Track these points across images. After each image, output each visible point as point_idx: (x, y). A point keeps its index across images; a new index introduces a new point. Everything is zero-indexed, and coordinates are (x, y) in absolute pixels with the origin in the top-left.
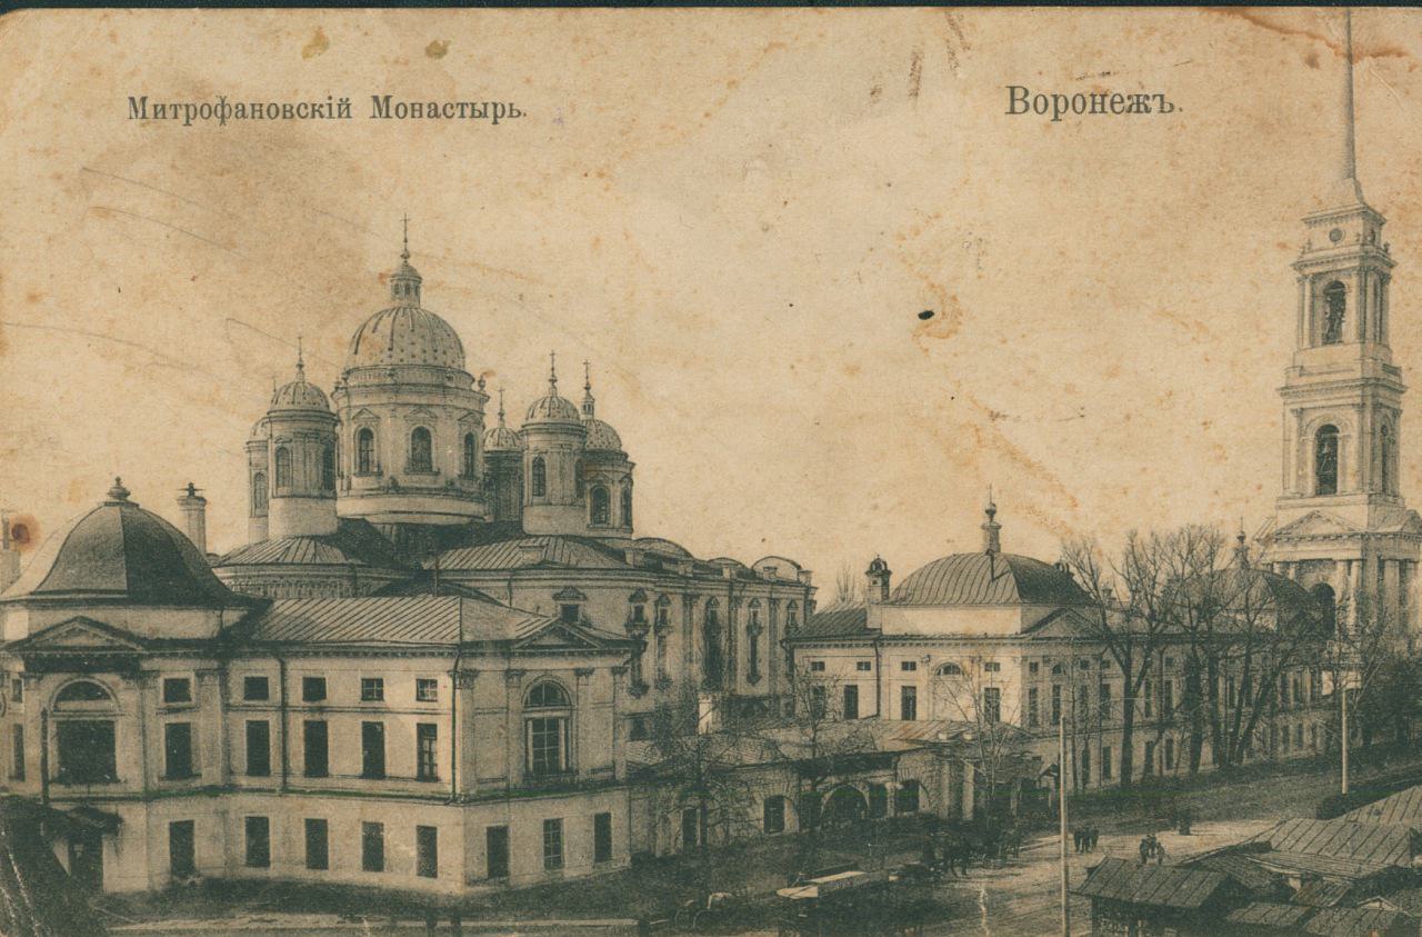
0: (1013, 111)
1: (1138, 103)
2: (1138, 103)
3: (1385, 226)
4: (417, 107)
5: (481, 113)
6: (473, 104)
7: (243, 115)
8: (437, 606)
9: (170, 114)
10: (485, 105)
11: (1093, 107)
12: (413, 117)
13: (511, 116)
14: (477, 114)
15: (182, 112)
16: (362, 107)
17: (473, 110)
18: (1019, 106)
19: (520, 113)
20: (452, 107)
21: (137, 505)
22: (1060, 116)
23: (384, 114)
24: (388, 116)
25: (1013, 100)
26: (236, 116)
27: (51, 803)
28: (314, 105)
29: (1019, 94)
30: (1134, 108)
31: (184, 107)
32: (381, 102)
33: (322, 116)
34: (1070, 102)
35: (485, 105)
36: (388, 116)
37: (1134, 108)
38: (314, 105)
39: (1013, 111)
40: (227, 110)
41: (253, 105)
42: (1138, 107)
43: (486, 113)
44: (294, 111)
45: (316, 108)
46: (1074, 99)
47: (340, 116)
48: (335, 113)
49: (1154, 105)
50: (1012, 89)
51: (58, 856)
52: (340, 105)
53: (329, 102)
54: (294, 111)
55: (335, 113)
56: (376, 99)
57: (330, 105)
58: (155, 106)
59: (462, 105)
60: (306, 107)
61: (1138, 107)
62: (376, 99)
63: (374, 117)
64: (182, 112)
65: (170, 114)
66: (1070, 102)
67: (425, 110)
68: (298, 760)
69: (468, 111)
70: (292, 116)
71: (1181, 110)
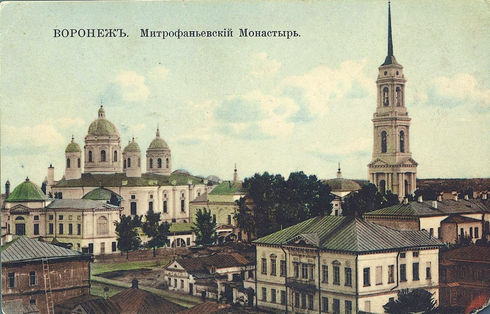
0: (55, 36)
1: (111, 33)
2: (111, 33)
3: (403, 69)
4: (192, 33)
5: (282, 35)
6: (279, 32)
7: (187, 36)
8: (422, 237)
9: (157, 34)
10: (284, 32)
11: (256, 35)
12: (89, 36)
13: (295, 36)
14: (281, 35)
15: (161, 35)
16: (236, 33)
17: (279, 34)
18: (57, 35)
19: (125, 35)
20: (271, 33)
21: (424, 229)
22: (165, 37)
23: (244, 35)
24: (246, 36)
25: (55, 33)
26: (184, 36)
27: (46, 206)
28: (219, 32)
29: (57, 31)
30: (109, 35)
31: (278, 33)
32: (243, 31)
33: (222, 36)
34: (168, 34)
35: (284, 32)
36: (246, 36)
37: (109, 35)
38: (219, 32)
39: (55, 36)
40: (180, 33)
41: (190, 32)
42: (111, 35)
43: (284, 35)
44: (212, 34)
45: (220, 33)
46: (170, 33)
47: (191, 36)
48: (227, 34)
49: (118, 33)
50: (55, 30)
51: (233, 292)
52: (228, 32)
53: (225, 31)
54: (212, 34)
55: (227, 34)
56: (142, 30)
57: (225, 32)
58: (151, 32)
59: (275, 32)
60: (216, 33)
61: (111, 35)
62: (142, 30)
63: (241, 36)
64: (161, 35)
65: (157, 34)
66: (168, 34)
67: (261, 34)
68: (58, 232)
69: (277, 34)
70: (211, 35)
71: (128, 36)
